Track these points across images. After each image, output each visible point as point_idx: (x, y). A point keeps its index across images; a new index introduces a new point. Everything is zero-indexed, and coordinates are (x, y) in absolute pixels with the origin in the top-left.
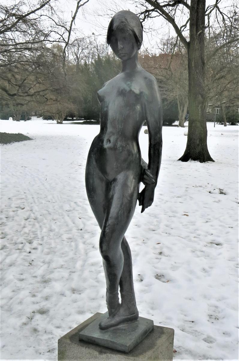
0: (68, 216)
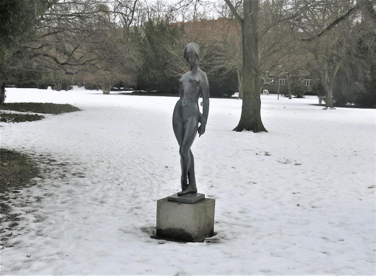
0: (140, 166)
